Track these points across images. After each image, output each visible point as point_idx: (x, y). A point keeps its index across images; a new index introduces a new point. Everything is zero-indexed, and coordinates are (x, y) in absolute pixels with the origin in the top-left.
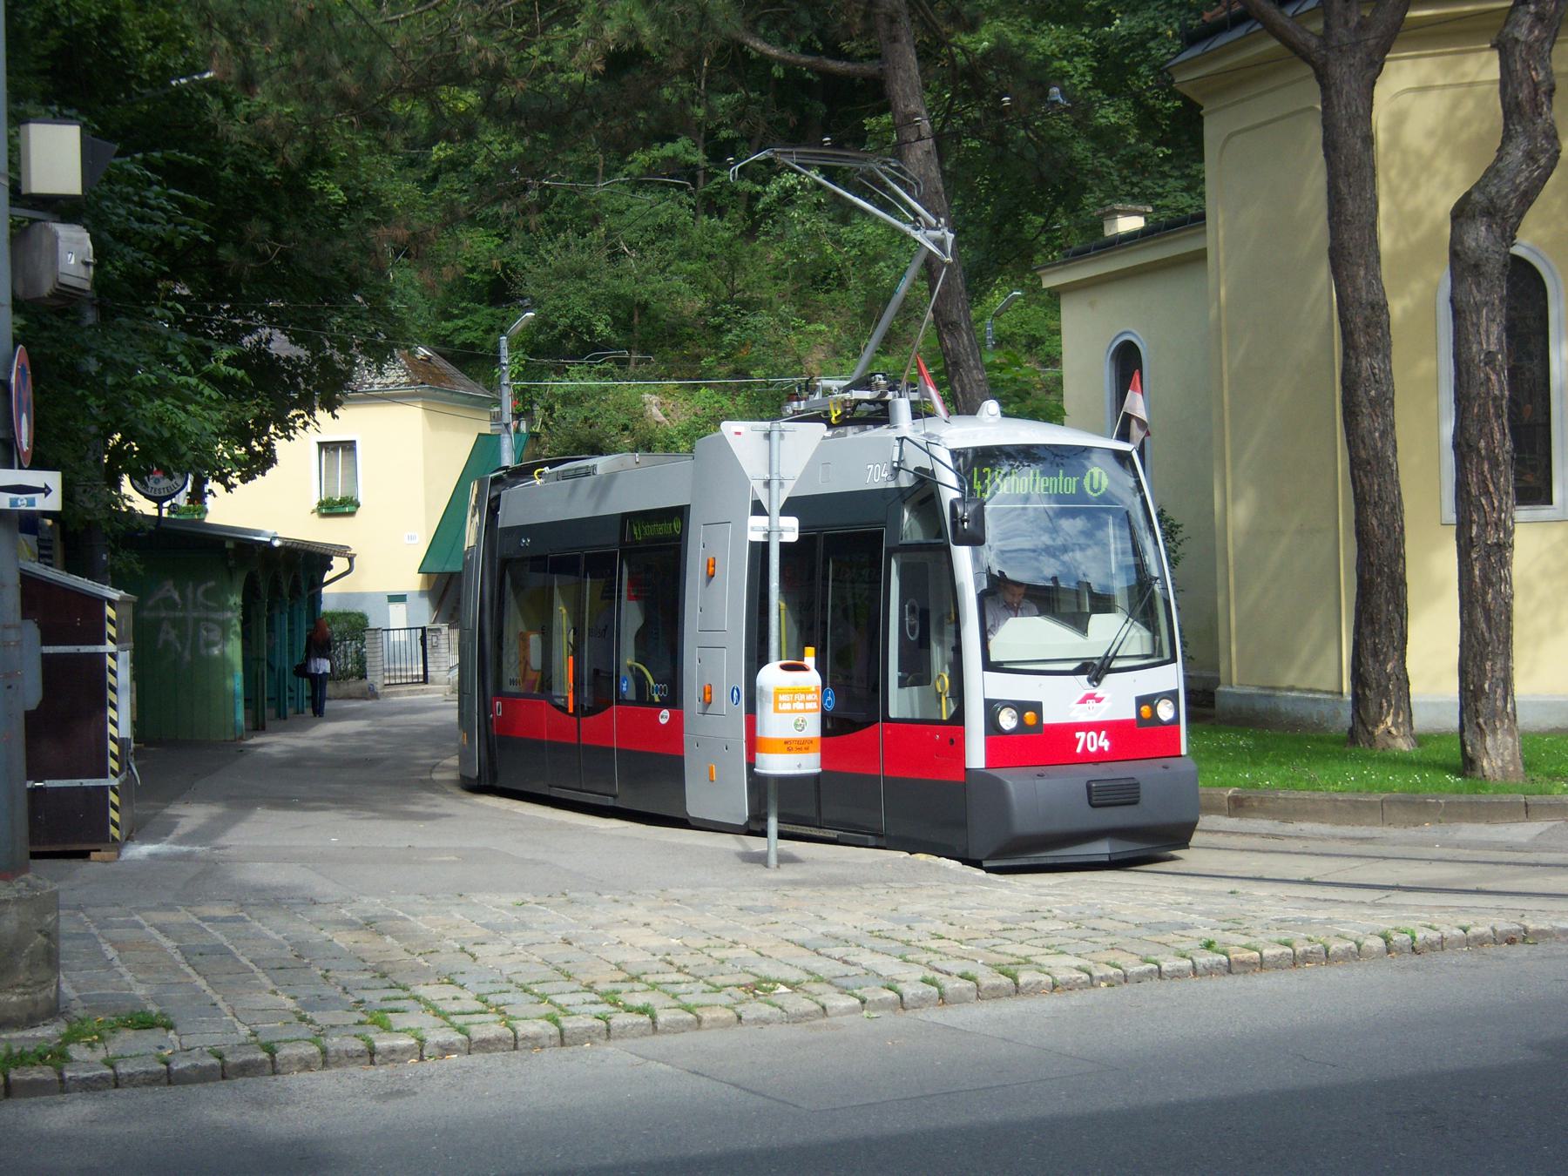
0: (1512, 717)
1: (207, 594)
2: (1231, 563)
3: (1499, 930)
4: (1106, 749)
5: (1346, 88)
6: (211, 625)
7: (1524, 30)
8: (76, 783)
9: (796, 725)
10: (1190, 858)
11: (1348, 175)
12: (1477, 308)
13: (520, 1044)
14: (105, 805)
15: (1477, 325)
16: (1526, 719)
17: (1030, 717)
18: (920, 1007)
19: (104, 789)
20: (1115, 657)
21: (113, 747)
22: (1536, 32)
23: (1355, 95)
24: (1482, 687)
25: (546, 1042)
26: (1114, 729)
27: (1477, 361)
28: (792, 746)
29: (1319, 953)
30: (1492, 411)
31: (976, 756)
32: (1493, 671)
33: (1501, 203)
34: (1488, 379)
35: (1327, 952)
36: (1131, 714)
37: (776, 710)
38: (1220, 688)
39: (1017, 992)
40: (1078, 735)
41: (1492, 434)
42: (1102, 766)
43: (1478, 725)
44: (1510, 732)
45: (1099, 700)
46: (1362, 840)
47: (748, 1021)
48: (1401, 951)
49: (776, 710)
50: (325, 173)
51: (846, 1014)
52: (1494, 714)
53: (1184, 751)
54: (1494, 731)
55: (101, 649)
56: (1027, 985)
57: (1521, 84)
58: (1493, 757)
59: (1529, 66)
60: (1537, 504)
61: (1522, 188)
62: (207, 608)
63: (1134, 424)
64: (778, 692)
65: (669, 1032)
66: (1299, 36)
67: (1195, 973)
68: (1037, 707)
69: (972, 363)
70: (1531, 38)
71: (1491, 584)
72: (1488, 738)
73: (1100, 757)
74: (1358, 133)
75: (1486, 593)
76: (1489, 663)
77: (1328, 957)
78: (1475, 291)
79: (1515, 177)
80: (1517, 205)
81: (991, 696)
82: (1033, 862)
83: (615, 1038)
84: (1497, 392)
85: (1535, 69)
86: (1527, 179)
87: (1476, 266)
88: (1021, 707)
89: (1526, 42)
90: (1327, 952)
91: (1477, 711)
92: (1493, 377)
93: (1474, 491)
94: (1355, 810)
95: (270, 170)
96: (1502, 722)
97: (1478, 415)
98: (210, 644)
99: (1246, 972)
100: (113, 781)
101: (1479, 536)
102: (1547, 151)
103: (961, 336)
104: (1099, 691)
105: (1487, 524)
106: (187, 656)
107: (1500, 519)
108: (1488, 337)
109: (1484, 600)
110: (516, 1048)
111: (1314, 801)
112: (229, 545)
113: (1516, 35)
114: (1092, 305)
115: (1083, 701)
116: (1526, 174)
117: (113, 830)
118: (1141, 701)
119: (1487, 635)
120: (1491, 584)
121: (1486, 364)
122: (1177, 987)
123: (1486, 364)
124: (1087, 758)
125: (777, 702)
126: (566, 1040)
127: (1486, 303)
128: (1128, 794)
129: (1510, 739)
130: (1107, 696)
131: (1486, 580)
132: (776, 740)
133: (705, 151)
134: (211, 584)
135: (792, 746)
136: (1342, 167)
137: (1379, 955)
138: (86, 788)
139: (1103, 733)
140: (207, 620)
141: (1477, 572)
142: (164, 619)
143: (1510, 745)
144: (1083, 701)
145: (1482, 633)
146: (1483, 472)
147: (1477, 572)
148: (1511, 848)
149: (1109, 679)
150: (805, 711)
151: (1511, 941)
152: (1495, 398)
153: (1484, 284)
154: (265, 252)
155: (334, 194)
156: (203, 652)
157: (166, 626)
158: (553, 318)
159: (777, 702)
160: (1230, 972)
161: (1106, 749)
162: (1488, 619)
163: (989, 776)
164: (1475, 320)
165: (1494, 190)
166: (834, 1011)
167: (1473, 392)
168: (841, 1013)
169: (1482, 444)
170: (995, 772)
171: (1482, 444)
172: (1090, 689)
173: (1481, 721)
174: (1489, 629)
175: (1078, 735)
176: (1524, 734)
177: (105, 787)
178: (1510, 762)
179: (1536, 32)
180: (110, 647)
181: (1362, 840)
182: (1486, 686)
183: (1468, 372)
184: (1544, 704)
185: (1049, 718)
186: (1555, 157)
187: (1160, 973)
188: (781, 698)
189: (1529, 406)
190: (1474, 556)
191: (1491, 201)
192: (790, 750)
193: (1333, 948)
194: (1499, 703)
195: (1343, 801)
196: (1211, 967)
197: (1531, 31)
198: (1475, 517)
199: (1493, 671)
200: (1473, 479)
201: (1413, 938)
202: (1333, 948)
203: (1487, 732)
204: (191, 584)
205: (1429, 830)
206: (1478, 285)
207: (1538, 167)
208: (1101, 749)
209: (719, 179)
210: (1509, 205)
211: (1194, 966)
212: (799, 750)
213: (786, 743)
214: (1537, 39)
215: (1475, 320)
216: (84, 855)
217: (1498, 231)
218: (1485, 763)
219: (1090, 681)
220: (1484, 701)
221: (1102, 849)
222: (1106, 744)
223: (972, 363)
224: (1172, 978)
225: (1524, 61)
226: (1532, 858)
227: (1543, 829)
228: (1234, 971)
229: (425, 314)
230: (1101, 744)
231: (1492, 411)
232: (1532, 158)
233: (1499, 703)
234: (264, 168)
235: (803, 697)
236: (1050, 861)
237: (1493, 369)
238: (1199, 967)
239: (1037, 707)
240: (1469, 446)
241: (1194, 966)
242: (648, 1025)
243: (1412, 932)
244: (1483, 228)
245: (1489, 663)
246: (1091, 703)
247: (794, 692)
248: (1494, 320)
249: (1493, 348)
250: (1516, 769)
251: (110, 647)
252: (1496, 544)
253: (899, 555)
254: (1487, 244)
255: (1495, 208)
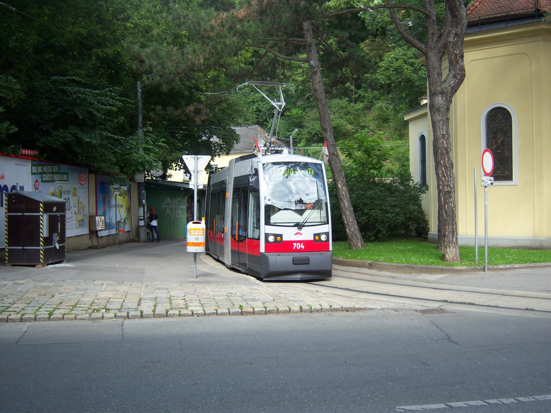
0: (455, 243)
1: (178, 201)
2: (432, 197)
3: (343, 307)
4: (303, 248)
5: (432, 59)
6: (179, 209)
7: (452, 38)
8: (15, 248)
9: (196, 239)
10: (334, 281)
11: (433, 84)
12: (439, 121)
13: (9, 321)
14: (40, 253)
15: (439, 126)
16: (460, 242)
17: (279, 238)
18: (134, 318)
19: (39, 250)
20: (306, 222)
21: (41, 239)
22: (456, 39)
23: (435, 61)
24: (445, 233)
25: (16, 320)
26: (305, 242)
27: (439, 137)
28: (194, 244)
29: (275, 310)
30: (444, 152)
31: (262, 249)
32: (448, 229)
33: (445, 90)
34: (443, 142)
35: (278, 311)
36: (312, 238)
37: (190, 235)
38: (429, 232)
39: (167, 316)
40: (294, 244)
41: (445, 158)
42: (300, 253)
43: (445, 244)
44: (455, 247)
45: (301, 234)
46: (393, 277)
47: (78, 319)
48: (305, 312)
49: (190, 235)
50: (200, 93)
51: (109, 319)
52: (449, 242)
53: (331, 249)
54: (450, 247)
55: (38, 214)
56: (170, 314)
57: (452, 55)
58: (449, 254)
59: (454, 49)
60: (509, 180)
61: (452, 85)
62: (178, 205)
63: (325, 156)
64: (191, 230)
65: (54, 320)
66: (419, 45)
67: (229, 314)
68: (281, 236)
69: (330, 140)
70: (454, 41)
71: (447, 203)
72: (448, 249)
73: (301, 250)
74: (436, 72)
75: (445, 206)
76: (447, 227)
77: (278, 312)
78: (438, 116)
79: (450, 82)
80: (451, 91)
81: (267, 232)
82: (278, 279)
83: (37, 321)
84: (446, 146)
85: (456, 50)
86: (454, 83)
87: (438, 109)
88: (276, 236)
89: (453, 42)
90: (278, 311)
91: (444, 241)
92: (445, 142)
93: (440, 176)
94: (397, 269)
95: (186, 93)
96: (452, 244)
97: (440, 153)
98: (178, 214)
99: (248, 315)
100: (41, 248)
101: (442, 189)
102: (460, 74)
103: (328, 133)
104: (301, 232)
105: (444, 185)
106: (173, 217)
107: (448, 184)
108: (443, 130)
109: (445, 208)
110: (7, 321)
111: (387, 265)
112: (182, 189)
113: (450, 40)
114: (415, 125)
115: (296, 234)
116: (454, 81)
117: (41, 260)
118: (315, 235)
119: (446, 218)
120: (447, 203)
121: (442, 138)
122: (235, 318)
123: (442, 138)
124: (296, 250)
125: (190, 232)
126: (23, 320)
127: (442, 120)
128: (306, 262)
129: (454, 249)
130: (304, 233)
131: (445, 202)
132: (190, 243)
133: (355, 86)
134: (179, 199)
135: (194, 244)
136: (431, 82)
137: (297, 312)
138: (35, 249)
139: (302, 244)
140: (178, 208)
141: (442, 200)
142: (168, 207)
143: (455, 251)
144: (296, 234)
145: (445, 218)
146: (443, 170)
147: (442, 200)
148: (428, 282)
149: (304, 228)
150: (198, 235)
151: (347, 311)
152: (445, 148)
153: (441, 114)
154: (160, 113)
155: (202, 98)
156: (177, 216)
157: (168, 209)
158: (311, 131)
159: (190, 232)
160: (242, 314)
161: (303, 248)
162: (446, 214)
163: (265, 255)
164: (438, 125)
165: (443, 86)
166: (106, 318)
167: (439, 146)
168: (108, 319)
169: (442, 162)
170: (267, 254)
171: (442, 162)
172: (298, 231)
173: (446, 244)
174: (447, 216)
175: (294, 244)
176: (461, 248)
177: (39, 249)
178: (454, 256)
179: (456, 39)
180: (41, 213)
181: (393, 277)
182: (447, 233)
183: (437, 141)
184: (509, 239)
185: (284, 239)
186: (464, 76)
187: (217, 314)
188: (192, 231)
189: (507, 152)
190: (441, 195)
191: (442, 89)
192: (194, 245)
193: (280, 310)
194: (451, 239)
195: (394, 266)
196: (235, 312)
197: (454, 39)
198: (441, 183)
199: (448, 229)
200: (440, 172)
201: (311, 308)
202: (280, 310)
203: (448, 247)
204: (174, 199)
205: (414, 276)
206: (439, 114)
207: (457, 79)
208: (301, 248)
209: (358, 94)
210: (448, 91)
211: (229, 312)
212: (197, 246)
213: (193, 243)
214: (456, 41)
215: (438, 125)
216: (34, 266)
217: (445, 99)
218: (447, 256)
219: (298, 229)
220: (446, 238)
221: (298, 277)
222: (303, 247)
223: (330, 140)
224: (221, 315)
225: (453, 48)
226: (434, 285)
227: (442, 277)
228: (243, 314)
229: (283, 130)
230: (301, 247)
231: (444, 152)
232: (455, 76)
233: (451, 239)
234: (185, 93)
235: (198, 231)
236: (283, 279)
237: (445, 139)
238: (231, 312)
239: (281, 236)
240: (439, 162)
241: (229, 312)
242: (47, 318)
243: (312, 306)
244: (440, 98)
245: (447, 227)
246: (298, 235)
247: (195, 230)
248: (444, 125)
249: (444, 133)
250: (457, 258)
251: (41, 213)
252: (447, 191)
253: (254, 193)
254: (441, 102)
255: (443, 92)
